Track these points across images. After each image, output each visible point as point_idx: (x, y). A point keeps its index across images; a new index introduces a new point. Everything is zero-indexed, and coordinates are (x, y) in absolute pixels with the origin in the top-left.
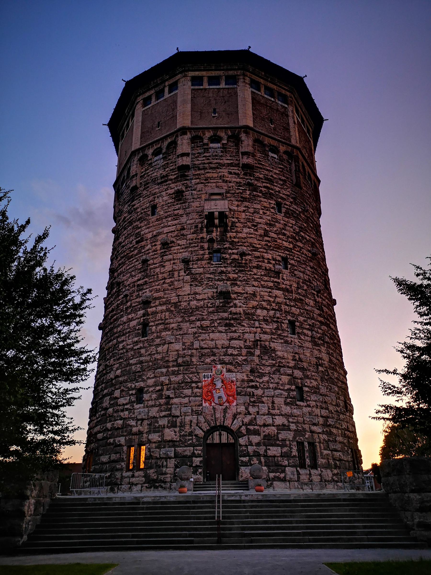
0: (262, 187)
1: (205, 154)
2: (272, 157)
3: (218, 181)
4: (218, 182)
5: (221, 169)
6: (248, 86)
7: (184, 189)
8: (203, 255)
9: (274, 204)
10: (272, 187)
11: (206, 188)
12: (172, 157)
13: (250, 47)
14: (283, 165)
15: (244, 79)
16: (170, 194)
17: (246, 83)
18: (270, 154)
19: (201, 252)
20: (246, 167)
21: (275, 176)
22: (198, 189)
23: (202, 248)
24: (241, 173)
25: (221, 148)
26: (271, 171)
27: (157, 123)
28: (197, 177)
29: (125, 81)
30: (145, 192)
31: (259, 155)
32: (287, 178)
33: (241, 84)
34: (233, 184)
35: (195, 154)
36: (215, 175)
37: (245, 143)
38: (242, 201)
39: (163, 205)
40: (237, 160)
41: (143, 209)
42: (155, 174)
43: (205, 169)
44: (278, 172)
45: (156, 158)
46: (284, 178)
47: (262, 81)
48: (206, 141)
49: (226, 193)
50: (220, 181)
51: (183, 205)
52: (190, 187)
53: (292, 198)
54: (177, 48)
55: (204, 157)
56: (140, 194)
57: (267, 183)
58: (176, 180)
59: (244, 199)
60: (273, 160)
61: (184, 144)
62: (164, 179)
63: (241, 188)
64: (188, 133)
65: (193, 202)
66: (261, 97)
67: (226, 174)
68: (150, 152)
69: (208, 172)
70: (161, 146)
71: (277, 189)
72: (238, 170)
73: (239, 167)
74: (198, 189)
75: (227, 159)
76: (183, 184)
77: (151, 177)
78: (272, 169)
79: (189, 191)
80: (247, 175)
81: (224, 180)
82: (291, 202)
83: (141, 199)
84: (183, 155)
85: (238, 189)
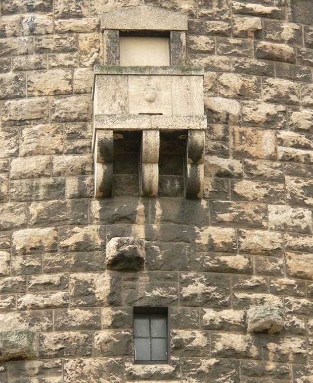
8: (91, 327)
19: (82, 315)
23: (85, 293)
65: (39, 68)
85: (245, 12)
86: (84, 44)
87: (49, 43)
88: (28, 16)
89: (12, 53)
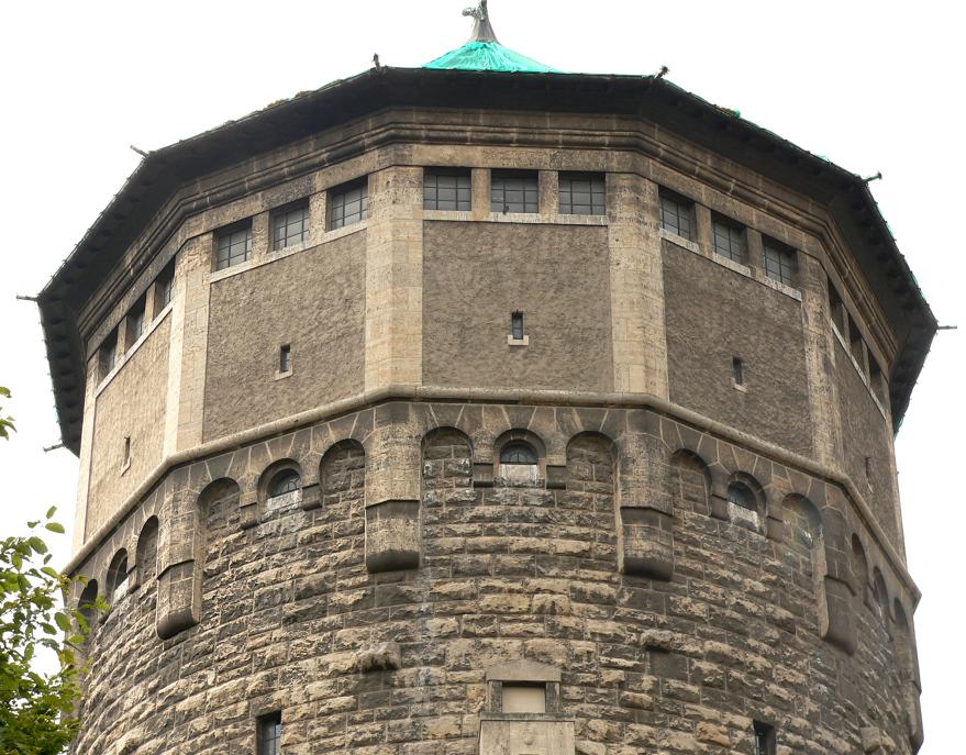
0: (699, 658)
1: (481, 509)
2: (741, 523)
3: (529, 627)
4: (530, 634)
5: (542, 575)
6: (648, 218)
7: (395, 657)
9: (747, 730)
10: (740, 656)
11: (484, 659)
12: (346, 510)
13: (665, 70)
14: (781, 557)
15: (636, 189)
16: (337, 673)
17: (644, 207)
18: (735, 511)
20: (639, 571)
21: (749, 605)
22: (451, 661)
24: (621, 595)
25: (541, 485)
26: (737, 586)
27: (277, 349)
28: (447, 605)
29: (141, 152)
30: (227, 647)
31: (688, 515)
32: (798, 611)
33: (624, 212)
34: (591, 646)
35: (438, 505)
36: (520, 603)
37: (640, 470)
38: (627, 720)
39: (307, 717)
40: (605, 539)
41: (218, 724)
42: (271, 573)
43: (479, 572)
44: (761, 588)
45: (272, 505)
46: (782, 613)
47: (702, 193)
48: (483, 452)
49: (562, 683)
50: (540, 629)
51: (393, 723)
52: (415, 648)
53: (816, 698)
54: (376, 57)
55: (472, 520)
56: (207, 652)
57: (720, 639)
58: (359, 615)
59: (635, 711)
60: (742, 536)
61: (391, 466)
62: (310, 603)
63: (622, 662)
64: (413, 416)
65: (433, 714)
66: (699, 266)
67: (562, 601)
68: (249, 471)
69: (490, 590)
70: (296, 453)
71: (760, 662)
72: (608, 581)
73: (614, 569)
74: (451, 661)
75: (568, 536)
76: (391, 634)
77: (254, 585)
78: (737, 578)
79: (413, 664)
80: (643, 607)
81: (553, 627)
82: (812, 717)
83: (211, 676)
84: (396, 507)
85: (610, 666)
86: (471, 694)
87: (442, 692)
88: (424, 669)
89: (409, 701)
